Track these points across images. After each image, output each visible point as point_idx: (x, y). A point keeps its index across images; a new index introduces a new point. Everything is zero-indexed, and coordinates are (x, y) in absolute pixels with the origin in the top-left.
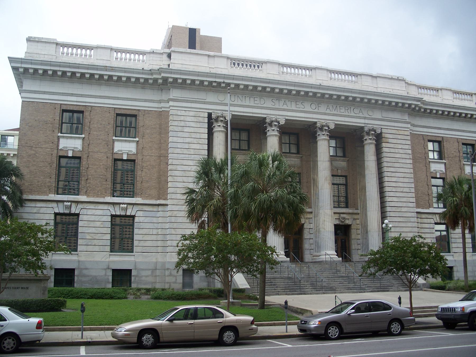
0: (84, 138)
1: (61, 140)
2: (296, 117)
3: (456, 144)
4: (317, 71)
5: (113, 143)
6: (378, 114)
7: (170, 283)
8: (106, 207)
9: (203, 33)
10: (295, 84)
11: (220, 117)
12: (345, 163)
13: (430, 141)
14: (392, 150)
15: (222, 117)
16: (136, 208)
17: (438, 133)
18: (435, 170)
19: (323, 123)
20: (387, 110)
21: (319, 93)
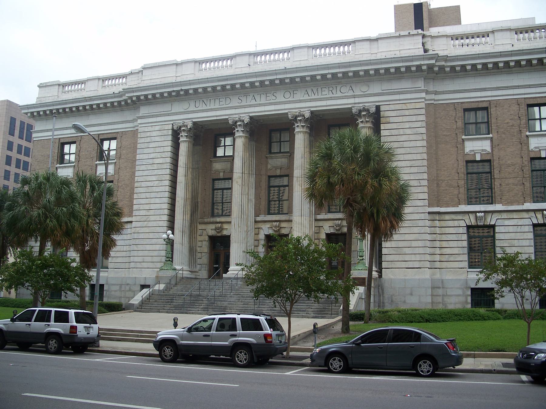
0: (492, 138)
1: (59, 170)
2: (265, 111)
3: (515, 108)
6: (376, 88)
8: (525, 215)
9: (428, 5)
10: (219, 79)
11: (299, 116)
14: (394, 132)
15: (184, 126)
16: (496, 216)
18: (471, 151)
19: (296, 112)
20: (389, 80)
21: (287, 78)
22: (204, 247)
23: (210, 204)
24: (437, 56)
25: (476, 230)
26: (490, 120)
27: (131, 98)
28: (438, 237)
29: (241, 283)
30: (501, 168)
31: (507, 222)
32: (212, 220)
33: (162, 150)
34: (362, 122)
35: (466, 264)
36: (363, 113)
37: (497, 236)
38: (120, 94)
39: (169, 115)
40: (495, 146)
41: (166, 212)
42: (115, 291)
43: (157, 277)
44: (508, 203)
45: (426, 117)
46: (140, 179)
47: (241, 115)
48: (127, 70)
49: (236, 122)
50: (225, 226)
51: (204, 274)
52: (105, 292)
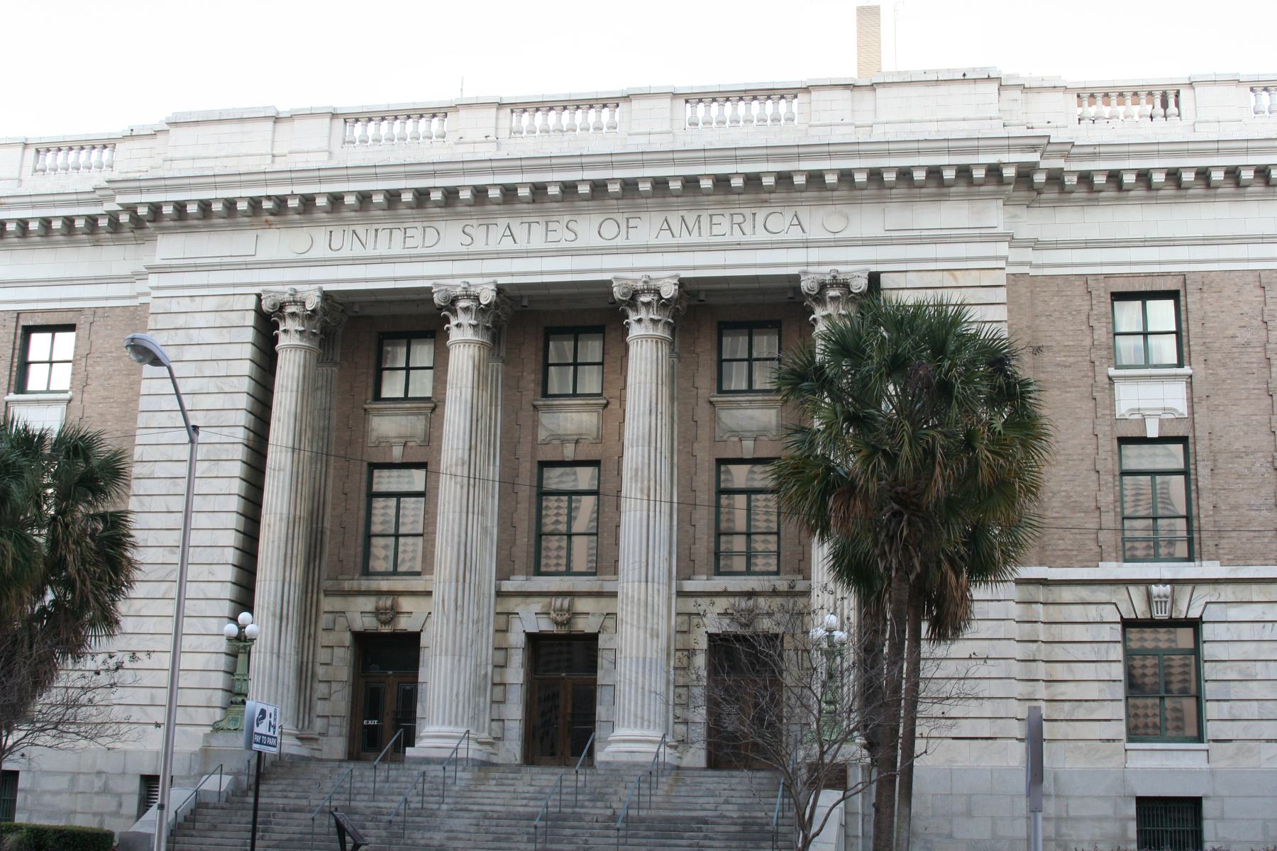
0: (70, 401)
1: (1122, 390)
2: (755, 266)
4: (636, 104)
5: (1112, 389)
7: (102, 814)
12: (773, 412)
13: (1119, 296)
15: (295, 302)
16: (1203, 594)
17: (1131, 263)
19: (636, 281)
22: (337, 664)
23: (360, 540)
24: (1045, 141)
25: (1148, 634)
26: (1184, 326)
27: (131, 209)
28: (1044, 652)
29: (467, 775)
30: (1215, 460)
31: (1234, 613)
32: (365, 584)
33: (222, 369)
34: (458, 326)
35: (1120, 730)
36: (832, 293)
37: (1208, 651)
38: (97, 195)
39: (247, 266)
40: (1200, 399)
41: (231, 556)
42: (56, 793)
43: (205, 752)
44: (1237, 558)
45: (1009, 311)
46: (150, 453)
47: (472, 281)
48: (117, 128)
49: (454, 300)
50: (406, 604)
51: (336, 746)
52: (20, 797)
